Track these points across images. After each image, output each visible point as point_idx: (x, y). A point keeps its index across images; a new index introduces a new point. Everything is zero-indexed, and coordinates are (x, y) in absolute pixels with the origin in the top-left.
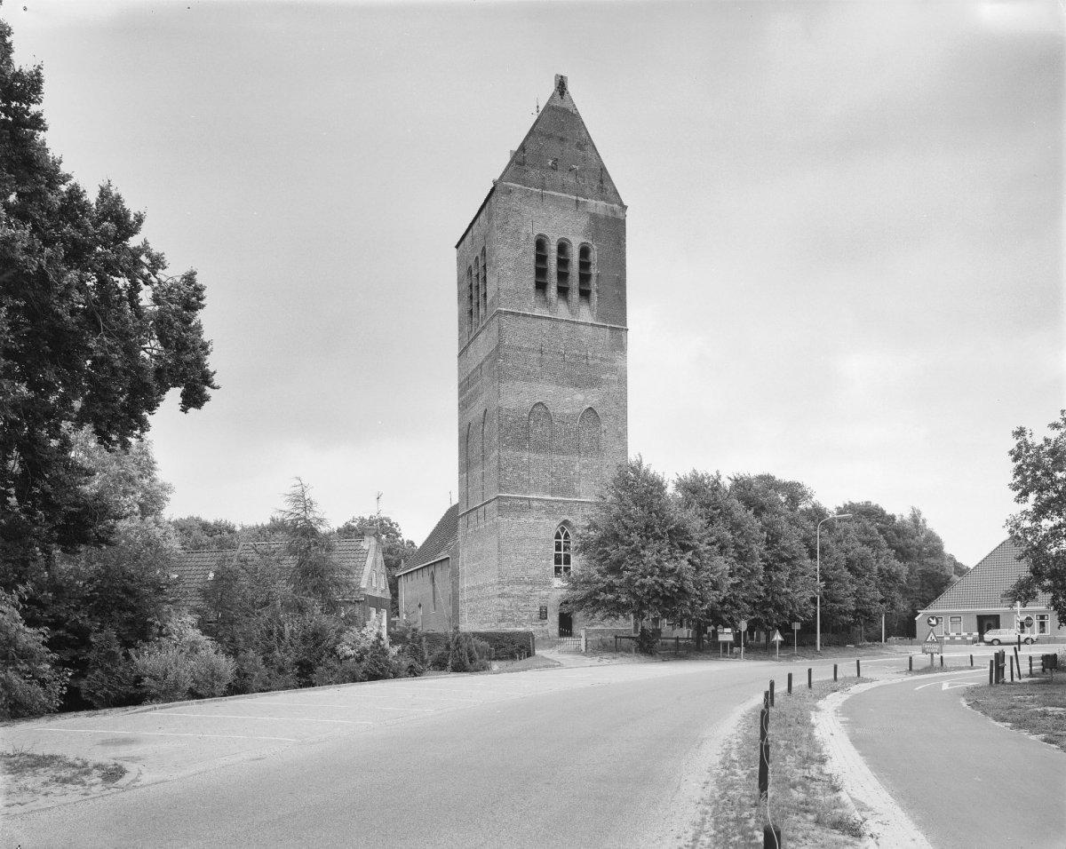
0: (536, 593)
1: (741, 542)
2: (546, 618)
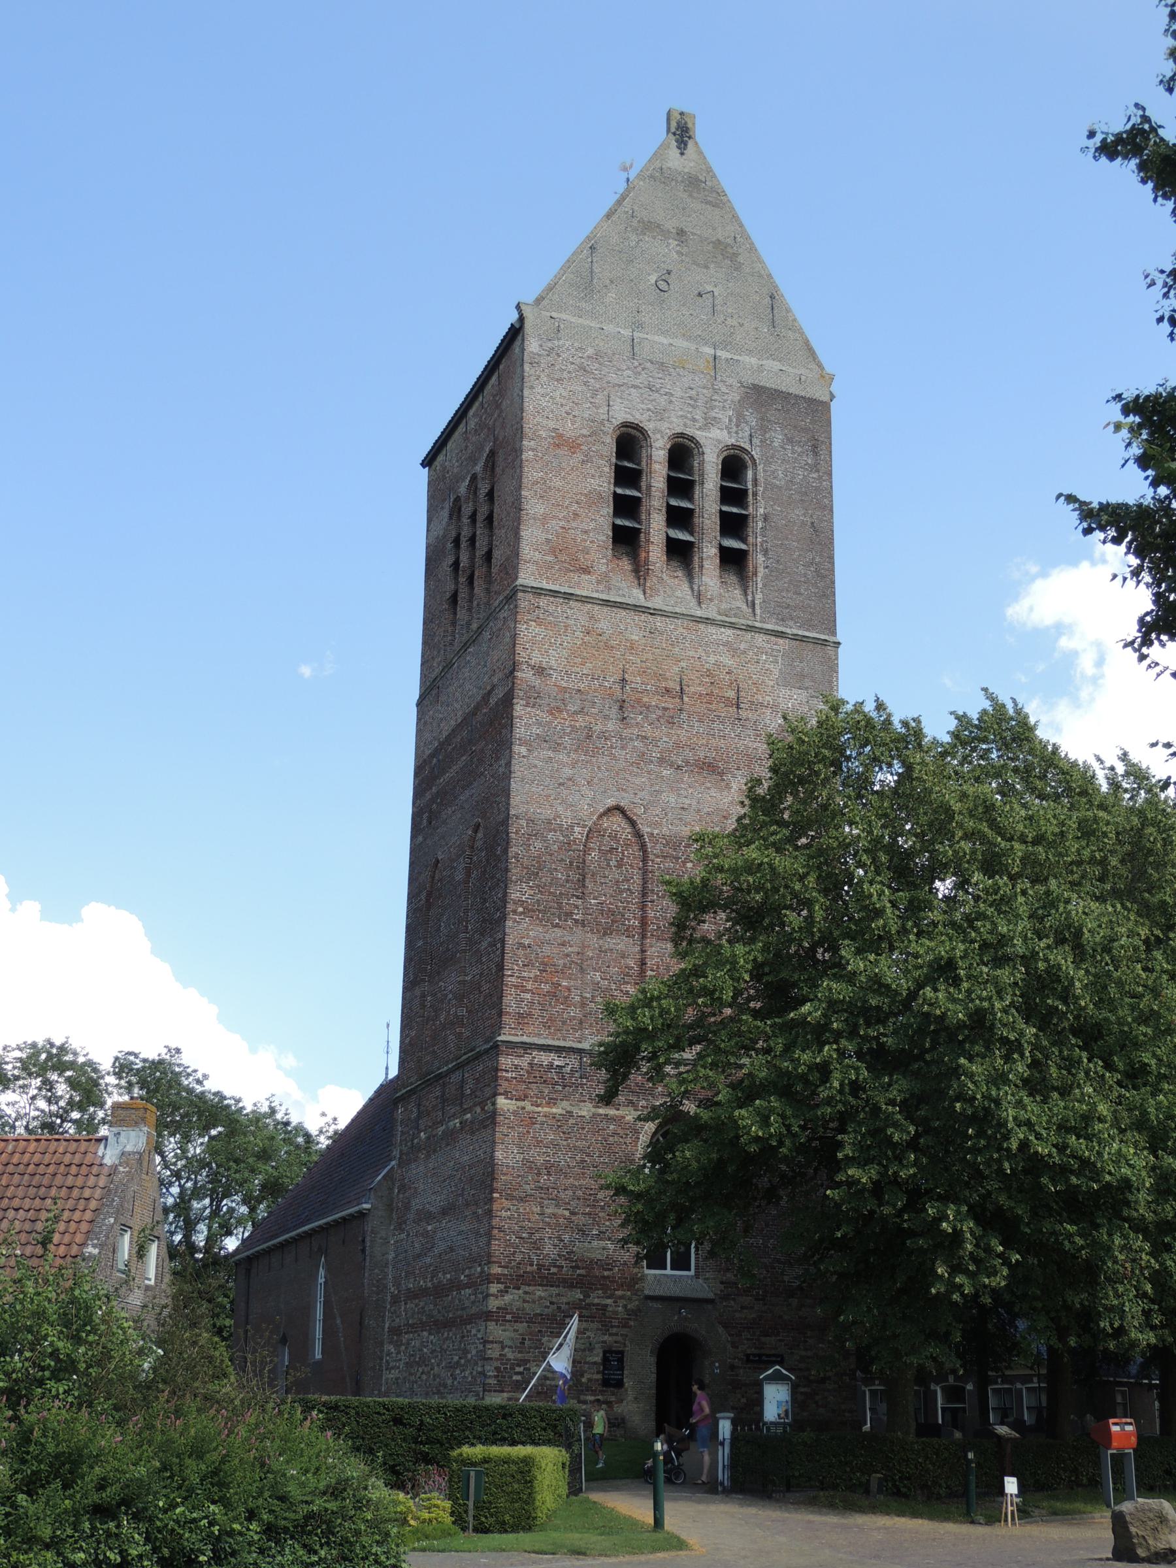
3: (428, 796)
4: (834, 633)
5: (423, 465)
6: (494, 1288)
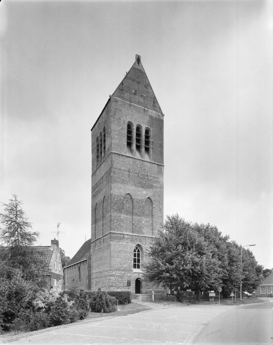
0: (126, 275)
1: (220, 253)
2: (130, 286)
4: (163, 164)
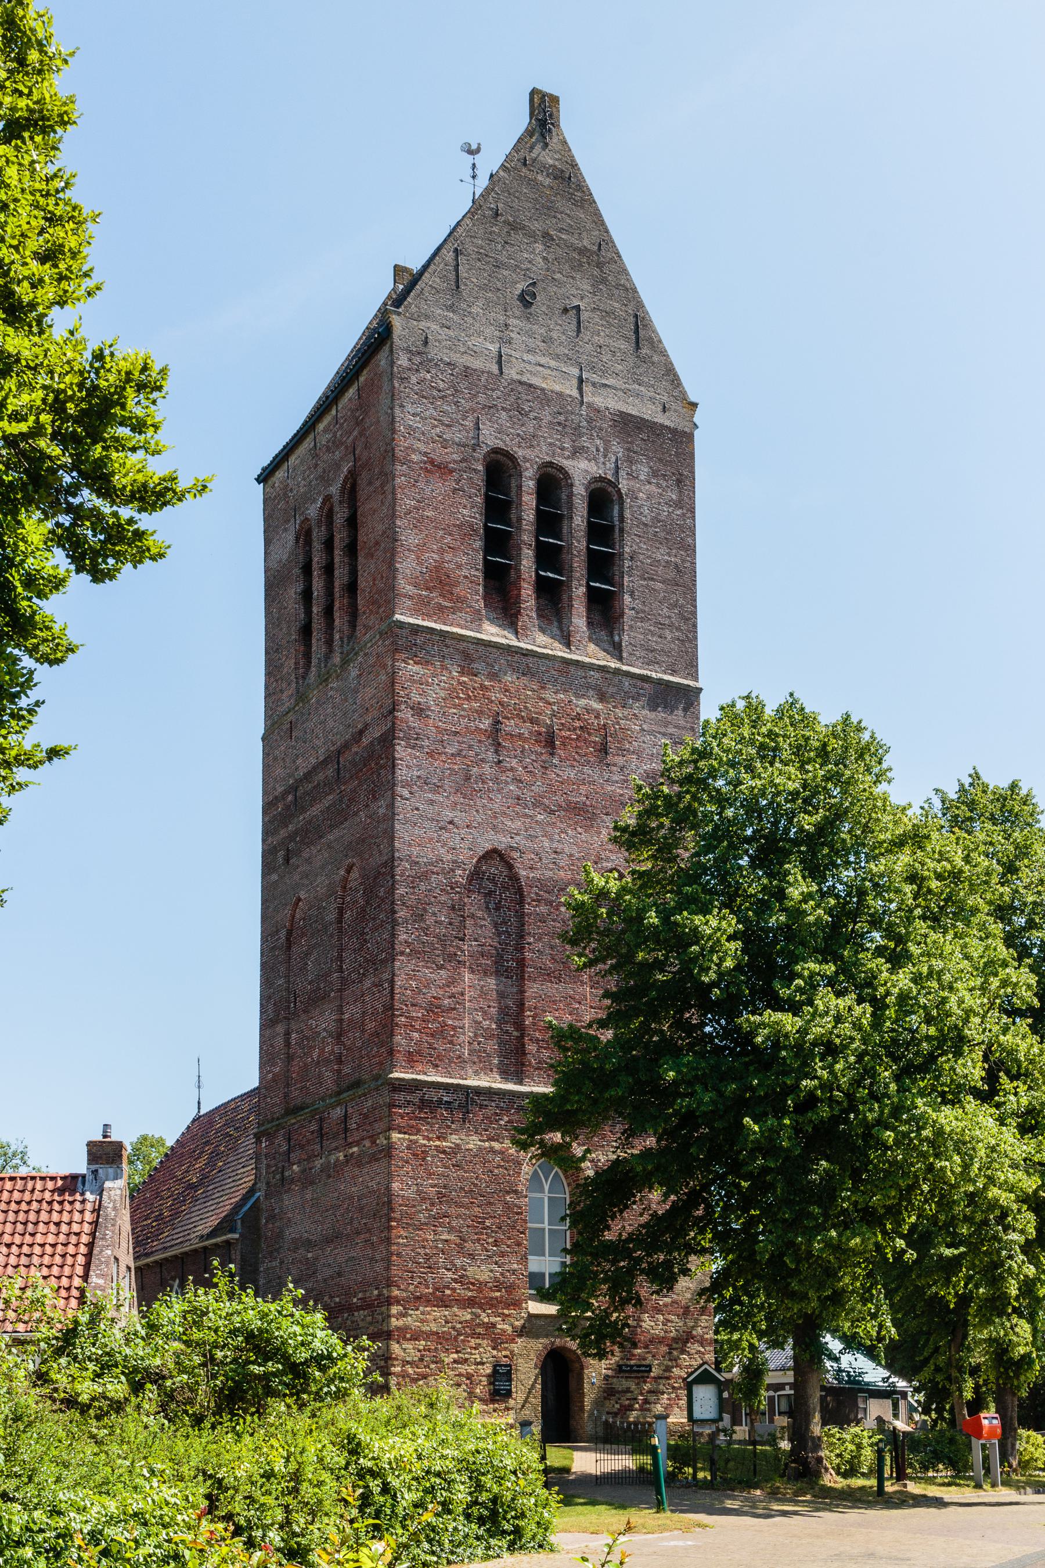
3: (283, 833)
5: (259, 480)
6: (395, 1310)
